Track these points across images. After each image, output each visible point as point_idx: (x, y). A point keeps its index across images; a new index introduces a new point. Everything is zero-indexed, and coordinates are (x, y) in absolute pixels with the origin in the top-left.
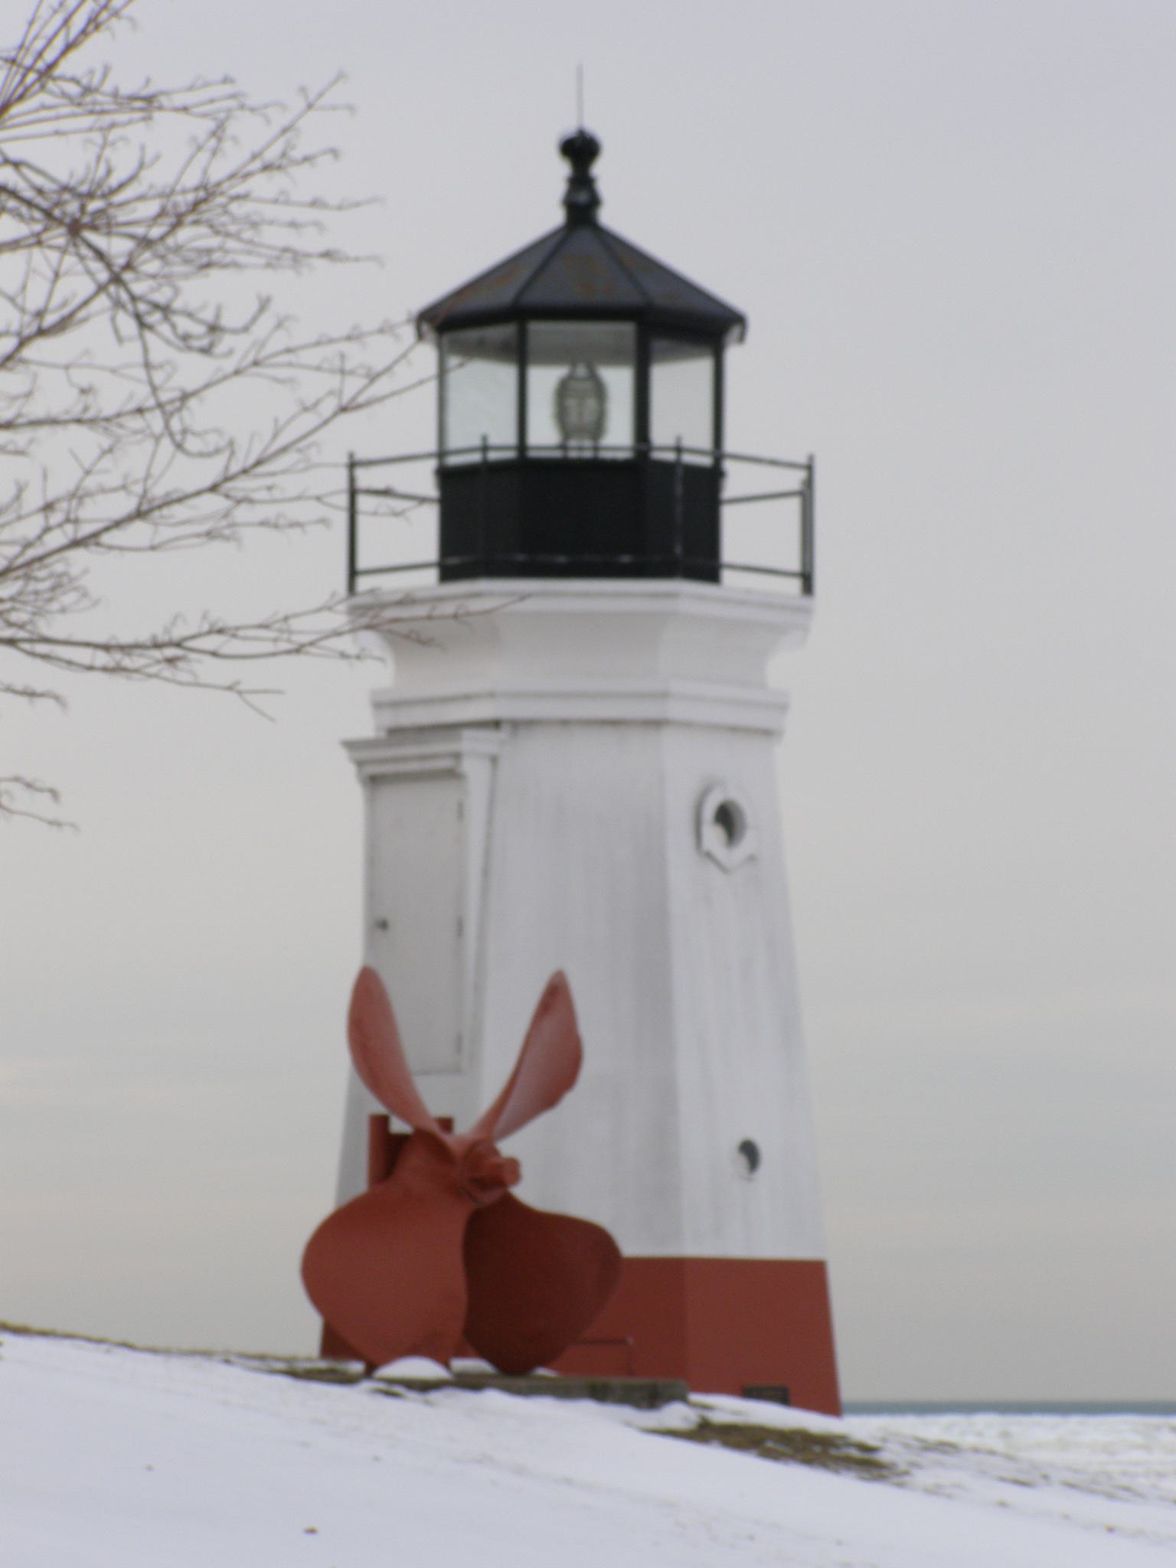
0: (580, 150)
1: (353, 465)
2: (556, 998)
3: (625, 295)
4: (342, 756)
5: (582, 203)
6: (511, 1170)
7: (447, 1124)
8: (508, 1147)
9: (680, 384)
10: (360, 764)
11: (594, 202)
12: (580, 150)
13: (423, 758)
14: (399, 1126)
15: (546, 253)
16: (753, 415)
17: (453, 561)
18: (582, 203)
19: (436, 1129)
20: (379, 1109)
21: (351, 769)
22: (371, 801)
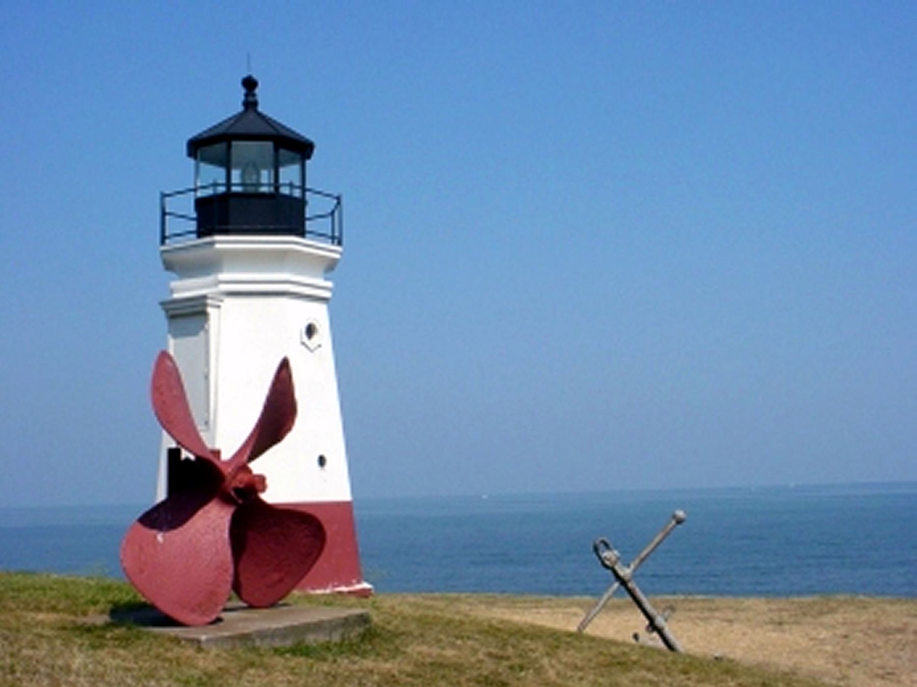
0: (250, 84)
1: (164, 196)
2: (285, 365)
3: (269, 130)
4: (159, 307)
5: (250, 104)
6: (259, 483)
7: (217, 453)
8: (257, 467)
9: (289, 174)
10: (167, 311)
11: (255, 104)
12: (250, 84)
13: (193, 306)
14: (185, 454)
15: (238, 118)
16: (320, 180)
17: (202, 230)
18: (250, 104)
19: (210, 457)
20: (173, 445)
21: (163, 313)
22: (170, 325)
